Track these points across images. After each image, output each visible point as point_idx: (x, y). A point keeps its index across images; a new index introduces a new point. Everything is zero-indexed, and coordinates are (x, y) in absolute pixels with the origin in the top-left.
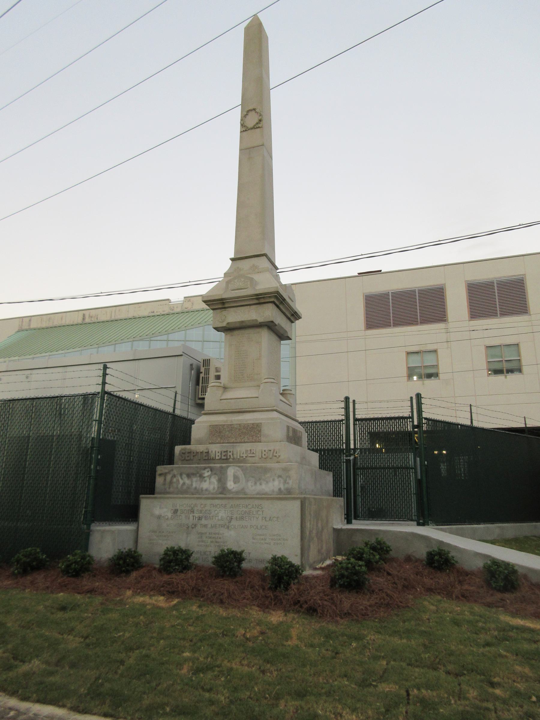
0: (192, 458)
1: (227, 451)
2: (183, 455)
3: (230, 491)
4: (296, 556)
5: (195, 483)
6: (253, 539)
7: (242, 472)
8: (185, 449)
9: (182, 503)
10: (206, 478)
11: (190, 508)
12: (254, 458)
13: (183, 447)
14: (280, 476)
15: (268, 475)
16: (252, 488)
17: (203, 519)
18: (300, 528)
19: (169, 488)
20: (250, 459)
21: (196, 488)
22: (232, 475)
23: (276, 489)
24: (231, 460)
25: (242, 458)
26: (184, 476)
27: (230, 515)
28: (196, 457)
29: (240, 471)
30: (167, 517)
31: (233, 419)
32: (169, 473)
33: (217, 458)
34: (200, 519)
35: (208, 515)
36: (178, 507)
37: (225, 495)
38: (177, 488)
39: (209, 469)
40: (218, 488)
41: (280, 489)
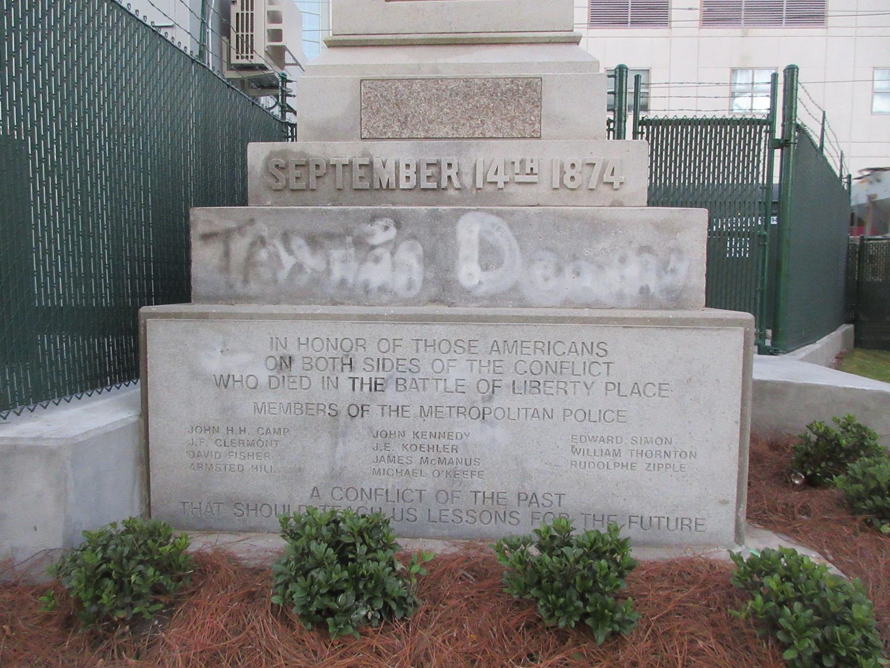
0: (313, 184)
1: (437, 164)
2: (281, 174)
3: (468, 295)
4: (724, 502)
5: (341, 264)
6: (574, 450)
7: (509, 234)
8: (283, 154)
9: (309, 336)
10: (378, 251)
11: (340, 353)
12: (533, 189)
13: (278, 146)
14: (644, 249)
15: (605, 243)
16: (545, 284)
17: (391, 390)
18: (738, 418)
19: (246, 281)
20: (520, 189)
21: (343, 282)
22: (475, 238)
23: (632, 290)
24: (451, 192)
25: (490, 188)
26: (298, 242)
27: (490, 377)
28: (327, 180)
29: (505, 227)
30: (252, 382)
31: (441, 61)
32: (240, 230)
33: (403, 184)
34: (376, 386)
35: (408, 376)
36: (292, 350)
37: (451, 305)
38: (276, 281)
39: (390, 221)
40: (425, 281)
41: (644, 290)
